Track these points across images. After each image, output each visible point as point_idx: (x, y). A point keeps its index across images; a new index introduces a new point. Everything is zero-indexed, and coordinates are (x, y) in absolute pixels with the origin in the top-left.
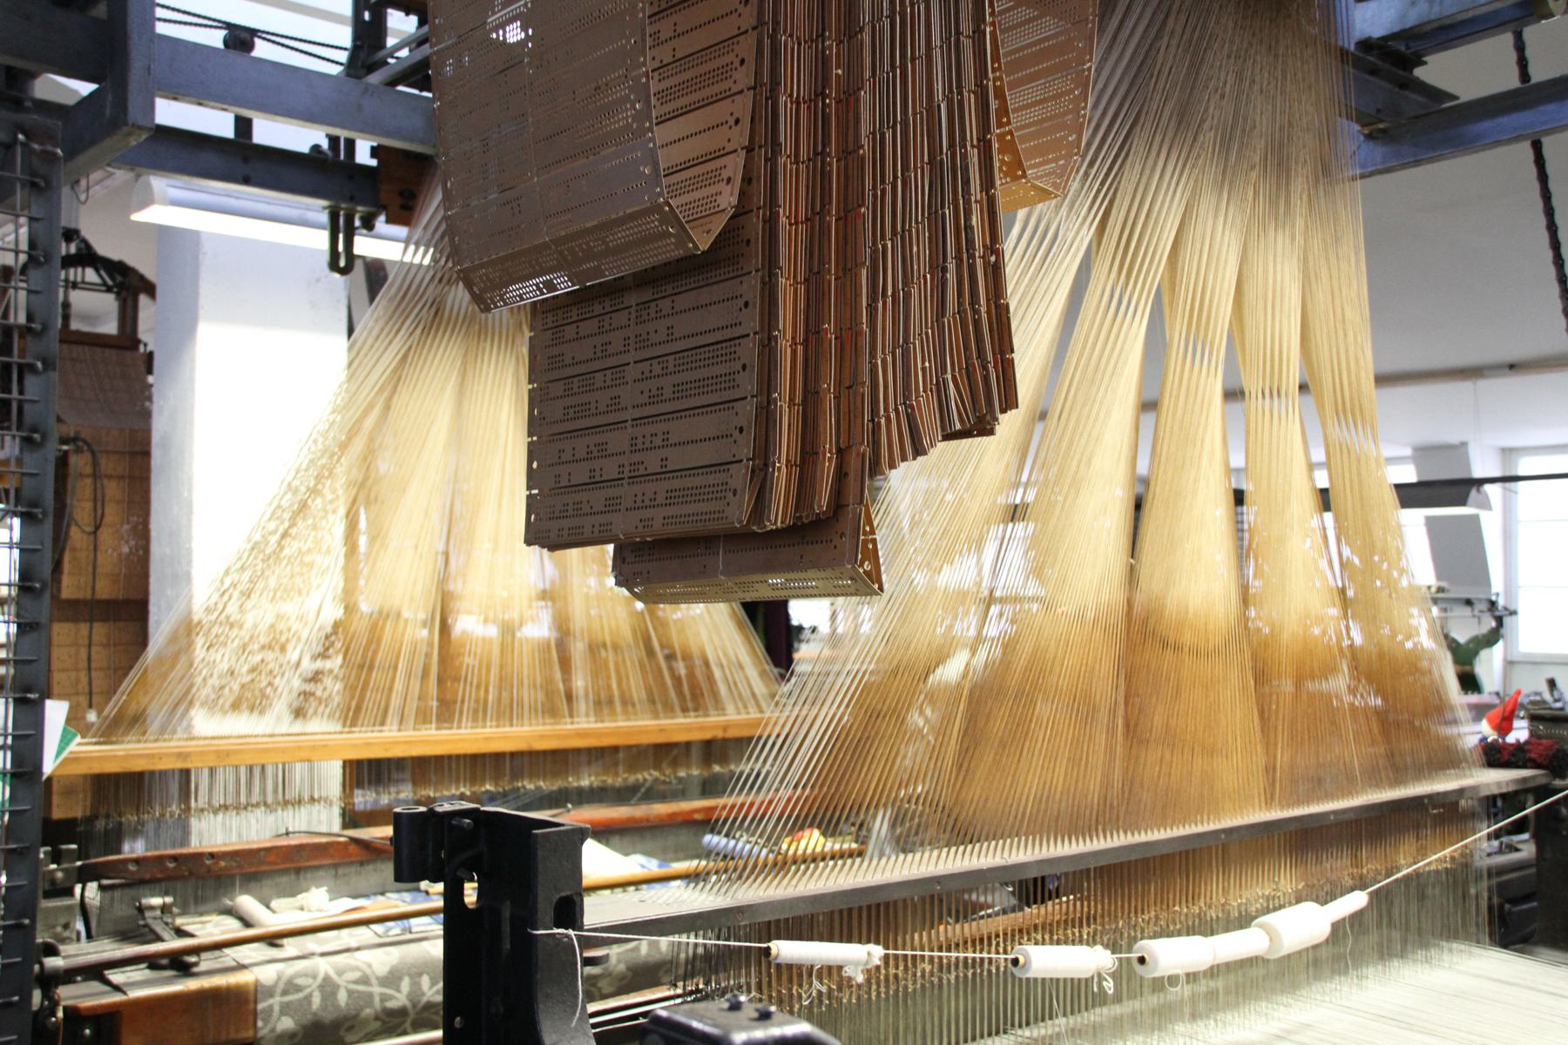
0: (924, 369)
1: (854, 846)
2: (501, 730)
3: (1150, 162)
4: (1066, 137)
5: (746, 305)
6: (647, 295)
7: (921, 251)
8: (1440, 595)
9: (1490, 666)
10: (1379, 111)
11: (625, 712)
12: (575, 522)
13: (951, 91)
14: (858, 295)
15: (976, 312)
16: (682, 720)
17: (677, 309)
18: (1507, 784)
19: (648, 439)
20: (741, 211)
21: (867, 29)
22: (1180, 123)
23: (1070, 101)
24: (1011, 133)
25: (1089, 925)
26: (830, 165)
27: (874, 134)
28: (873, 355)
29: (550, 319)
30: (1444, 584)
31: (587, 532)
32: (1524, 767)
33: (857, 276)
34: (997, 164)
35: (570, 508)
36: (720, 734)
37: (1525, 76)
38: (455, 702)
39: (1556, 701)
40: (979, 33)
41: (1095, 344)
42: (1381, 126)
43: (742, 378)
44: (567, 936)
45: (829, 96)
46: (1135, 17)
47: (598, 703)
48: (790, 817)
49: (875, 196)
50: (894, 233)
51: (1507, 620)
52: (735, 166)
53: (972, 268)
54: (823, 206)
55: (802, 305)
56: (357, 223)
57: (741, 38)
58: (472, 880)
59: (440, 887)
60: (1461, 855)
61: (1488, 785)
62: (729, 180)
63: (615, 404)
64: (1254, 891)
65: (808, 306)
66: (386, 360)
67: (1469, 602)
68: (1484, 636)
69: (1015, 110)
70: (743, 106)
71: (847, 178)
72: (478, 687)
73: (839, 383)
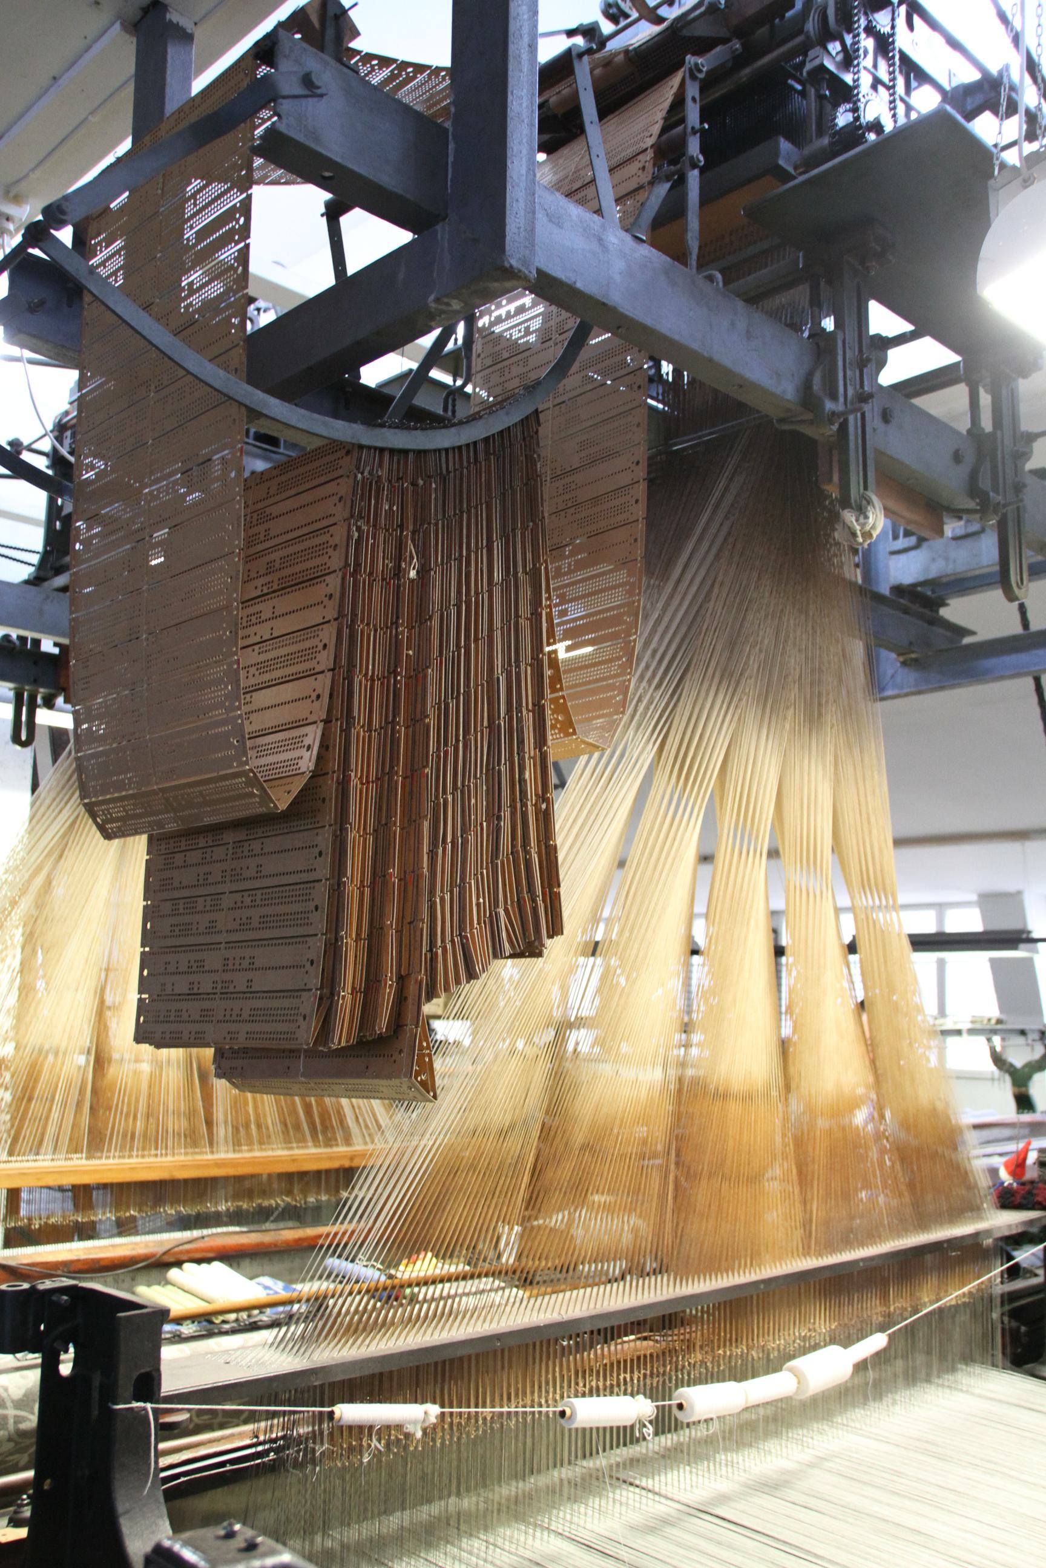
0: (478, 905)
1: (467, 1268)
2: (147, 1160)
4: (614, 697)
5: (320, 854)
6: (242, 835)
7: (479, 802)
8: (999, 1027)
10: (911, 643)
11: (261, 1143)
13: (510, 665)
14: (419, 842)
15: (527, 852)
16: (313, 1150)
17: (265, 850)
18: (1017, 1225)
19: (237, 961)
20: (318, 774)
26: (399, 732)
27: (439, 704)
28: (432, 893)
29: (163, 847)
30: (1003, 1017)
31: (185, 1036)
32: (1033, 1208)
34: (548, 724)
35: (173, 1014)
37: (1025, 624)
40: (536, 616)
42: (913, 656)
43: (315, 917)
44: (145, 1409)
45: (400, 674)
48: (410, 1240)
50: (455, 788)
52: (313, 735)
53: (524, 815)
54: (392, 767)
55: (370, 853)
56: (39, 701)
59: (36, 1358)
60: (978, 1290)
61: (1000, 1228)
63: (212, 928)
65: (375, 853)
66: (56, 826)
67: (1023, 1033)
69: (565, 672)
70: (323, 684)
71: (414, 742)
72: (128, 1115)
73: (401, 917)
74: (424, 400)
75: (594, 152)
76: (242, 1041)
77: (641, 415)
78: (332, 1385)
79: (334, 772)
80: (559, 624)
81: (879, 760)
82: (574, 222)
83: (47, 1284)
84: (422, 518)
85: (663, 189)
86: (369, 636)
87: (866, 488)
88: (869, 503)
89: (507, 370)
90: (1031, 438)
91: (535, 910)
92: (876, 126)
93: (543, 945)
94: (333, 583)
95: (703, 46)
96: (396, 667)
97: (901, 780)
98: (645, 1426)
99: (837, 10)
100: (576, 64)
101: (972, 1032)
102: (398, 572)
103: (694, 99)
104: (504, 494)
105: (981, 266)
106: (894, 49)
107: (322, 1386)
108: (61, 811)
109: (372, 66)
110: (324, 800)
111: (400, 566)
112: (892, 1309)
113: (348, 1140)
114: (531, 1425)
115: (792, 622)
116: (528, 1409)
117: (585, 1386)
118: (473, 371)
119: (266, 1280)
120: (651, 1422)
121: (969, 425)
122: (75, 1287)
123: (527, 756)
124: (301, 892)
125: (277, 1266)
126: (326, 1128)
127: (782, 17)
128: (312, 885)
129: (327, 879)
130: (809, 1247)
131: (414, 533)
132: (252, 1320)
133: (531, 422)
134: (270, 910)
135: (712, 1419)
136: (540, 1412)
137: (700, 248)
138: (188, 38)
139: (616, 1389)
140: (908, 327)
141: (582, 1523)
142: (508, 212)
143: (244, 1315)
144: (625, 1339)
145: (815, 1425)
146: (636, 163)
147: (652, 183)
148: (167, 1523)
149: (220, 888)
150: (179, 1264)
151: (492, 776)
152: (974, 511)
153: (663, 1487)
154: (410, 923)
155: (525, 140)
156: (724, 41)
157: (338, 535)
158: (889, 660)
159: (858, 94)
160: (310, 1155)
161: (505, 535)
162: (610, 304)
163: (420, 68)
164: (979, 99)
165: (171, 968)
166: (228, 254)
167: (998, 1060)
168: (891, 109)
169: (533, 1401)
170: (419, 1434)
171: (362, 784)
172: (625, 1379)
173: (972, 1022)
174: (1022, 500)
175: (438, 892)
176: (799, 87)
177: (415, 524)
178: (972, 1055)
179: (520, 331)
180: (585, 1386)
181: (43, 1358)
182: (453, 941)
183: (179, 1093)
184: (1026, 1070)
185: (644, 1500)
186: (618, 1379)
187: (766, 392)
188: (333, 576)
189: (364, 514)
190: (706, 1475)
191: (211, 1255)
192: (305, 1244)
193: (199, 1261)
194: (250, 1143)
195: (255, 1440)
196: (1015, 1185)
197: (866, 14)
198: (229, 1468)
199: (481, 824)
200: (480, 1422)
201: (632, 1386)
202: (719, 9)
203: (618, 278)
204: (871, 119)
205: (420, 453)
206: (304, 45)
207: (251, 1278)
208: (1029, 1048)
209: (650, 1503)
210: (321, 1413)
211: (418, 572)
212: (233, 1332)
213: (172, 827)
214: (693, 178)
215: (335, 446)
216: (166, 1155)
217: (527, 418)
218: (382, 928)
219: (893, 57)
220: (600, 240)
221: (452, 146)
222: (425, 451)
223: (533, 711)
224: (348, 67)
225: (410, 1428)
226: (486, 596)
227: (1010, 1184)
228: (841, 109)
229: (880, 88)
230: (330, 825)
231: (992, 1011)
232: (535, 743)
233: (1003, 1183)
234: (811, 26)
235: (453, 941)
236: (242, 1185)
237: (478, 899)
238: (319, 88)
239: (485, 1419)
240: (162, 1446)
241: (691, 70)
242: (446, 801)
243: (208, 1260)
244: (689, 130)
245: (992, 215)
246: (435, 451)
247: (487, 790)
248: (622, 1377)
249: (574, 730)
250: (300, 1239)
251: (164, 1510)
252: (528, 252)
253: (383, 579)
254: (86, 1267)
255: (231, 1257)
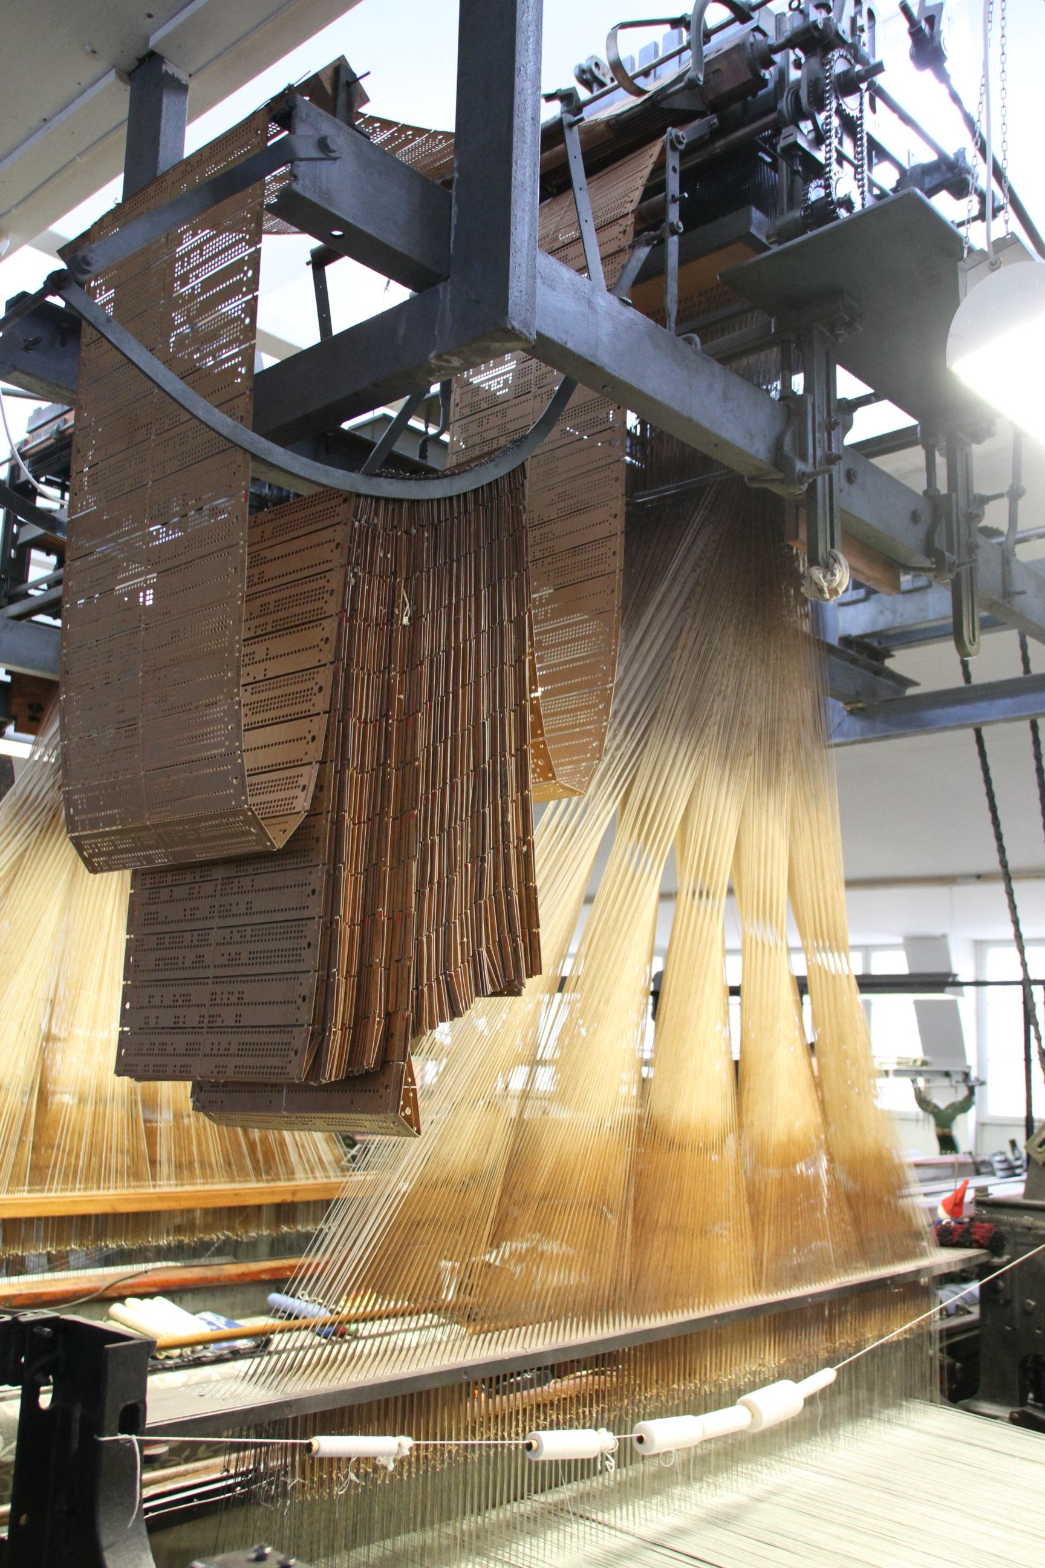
0: (462, 944)
2: (89, 1193)
3: (666, 747)
4: (591, 743)
5: (314, 892)
6: (231, 872)
7: (464, 844)
8: (924, 1068)
9: (964, 1129)
10: (858, 693)
11: (204, 1176)
12: (159, 1060)
14: (408, 883)
15: (508, 893)
16: (254, 1185)
18: (956, 1263)
19: (225, 997)
20: (313, 813)
21: (427, 663)
22: (690, 717)
23: (596, 713)
24: (544, 743)
25: (598, 1406)
26: (390, 774)
28: (419, 932)
29: (148, 881)
30: (928, 1058)
31: (170, 1070)
32: (970, 1247)
33: (408, 868)
36: (289, 1198)
38: (48, 1167)
39: (1017, 1159)
40: (520, 661)
41: (614, 904)
42: (860, 705)
43: (306, 954)
44: (130, 1441)
46: (654, 633)
47: (179, 1166)
49: (427, 799)
51: (977, 1089)
52: (309, 776)
54: (382, 808)
57: (320, 669)
58: (48, 1383)
59: (17, 1390)
62: (304, 788)
64: (740, 1366)
65: (366, 892)
67: (947, 1074)
68: (960, 1103)
69: (546, 716)
70: (318, 726)
72: (70, 1153)
73: (389, 958)
74: (407, 449)
75: (582, 218)
76: (230, 1075)
77: (621, 472)
78: (306, 1417)
79: (328, 812)
80: (541, 669)
81: (832, 807)
82: (567, 288)
83: (29, 1316)
84: (415, 566)
85: (643, 252)
86: (363, 679)
87: (832, 546)
88: (835, 561)
89: (485, 420)
90: (984, 500)
91: (515, 950)
92: (847, 203)
93: (523, 985)
94: (330, 627)
95: (682, 118)
96: (388, 710)
97: (852, 824)
98: (607, 1459)
99: (809, 92)
100: (567, 132)
101: (898, 1073)
102: (391, 618)
103: (674, 169)
104: (491, 544)
105: (950, 341)
106: (862, 131)
107: (295, 1419)
108: (8, 845)
109: (374, 129)
110: (318, 839)
111: (393, 612)
112: (837, 1345)
113: (291, 1174)
114: (494, 1458)
115: (754, 672)
116: (492, 1442)
117: (545, 1419)
118: (451, 419)
119: (209, 1316)
120: (613, 1455)
121: (925, 487)
122: (56, 1319)
123: (510, 799)
124: (293, 929)
125: (220, 1302)
126: (267, 1162)
127: (755, 95)
128: (304, 922)
129: (320, 917)
130: (760, 1282)
131: (406, 580)
132: (196, 1356)
133: (518, 474)
134: (261, 946)
135: (670, 1452)
136: (503, 1445)
137: (678, 312)
138: (183, 88)
139: (575, 1423)
140: (867, 390)
141: (541, 1557)
142: (511, 276)
143: (188, 1351)
144: (578, 1374)
145: (763, 1460)
146: (617, 227)
147: (632, 247)
148: (151, 1556)
149: (208, 924)
150: (121, 1299)
151: (478, 819)
152: (929, 570)
153: (619, 1521)
154: (397, 961)
155: (527, 208)
156: (701, 115)
157: (335, 581)
158: (837, 709)
159: (830, 172)
160: (252, 1189)
161: (491, 584)
162: (598, 363)
163: (419, 131)
164: (936, 179)
165: (156, 1001)
166: (233, 307)
167: (923, 1101)
168: (859, 187)
169: (496, 1434)
170: (391, 1467)
171: (354, 824)
172: (584, 1412)
173: (898, 1063)
174: (976, 561)
175: (425, 932)
176: (769, 160)
177: (407, 573)
178: (897, 1097)
179: (499, 383)
180: (545, 1419)
181: (23, 1389)
182: (438, 979)
183: (123, 1128)
184: (950, 1111)
185: (601, 1534)
186: (577, 1413)
187: (741, 452)
188: (329, 620)
189: (361, 560)
190: (660, 1509)
191: (154, 1290)
192: (248, 1279)
193: (142, 1296)
194: (193, 1176)
195: (225, 1474)
196: (953, 1224)
197: (837, 98)
198: (196, 1502)
199: (466, 866)
200: (446, 1455)
201: (591, 1419)
202: (698, 85)
203: (605, 339)
204: (842, 196)
205: (413, 503)
206: (313, 106)
207: (194, 1314)
208: (953, 1090)
209: (607, 1536)
210: (294, 1444)
211: (410, 619)
212: (177, 1368)
213: (162, 862)
214: (673, 242)
215: (330, 493)
216: (109, 1188)
217: (514, 470)
218: (371, 966)
219: (861, 139)
220: (590, 302)
221: (454, 209)
222: (418, 501)
223: (516, 756)
224: (353, 127)
225: (382, 1461)
226: (473, 643)
227: (948, 1223)
228: (813, 185)
229: (845, 163)
230: (324, 864)
231: (916, 1052)
232: (517, 787)
233: (941, 1222)
234: (784, 105)
235: (438, 979)
236: (183, 1220)
237: (462, 938)
238: (334, 151)
239: (450, 1452)
240: (147, 1476)
241: (672, 141)
242: (433, 842)
243: (151, 1295)
244: (670, 197)
245: (961, 294)
246: (427, 501)
247: (472, 832)
248: (580, 1411)
249: (554, 774)
250: (243, 1274)
251: (147, 1543)
252: (529, 314)
253: (377, 625)
254: (29, 1302)
255: (173, 1292)
